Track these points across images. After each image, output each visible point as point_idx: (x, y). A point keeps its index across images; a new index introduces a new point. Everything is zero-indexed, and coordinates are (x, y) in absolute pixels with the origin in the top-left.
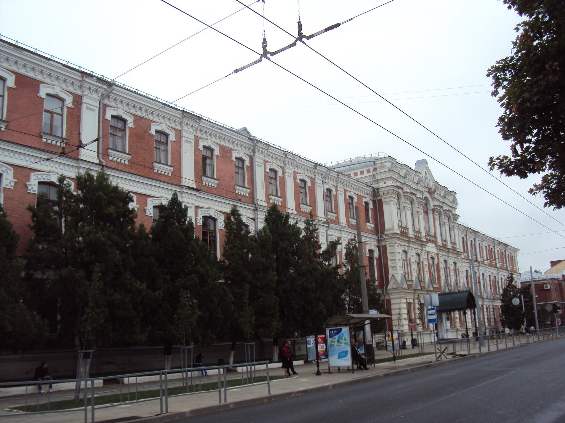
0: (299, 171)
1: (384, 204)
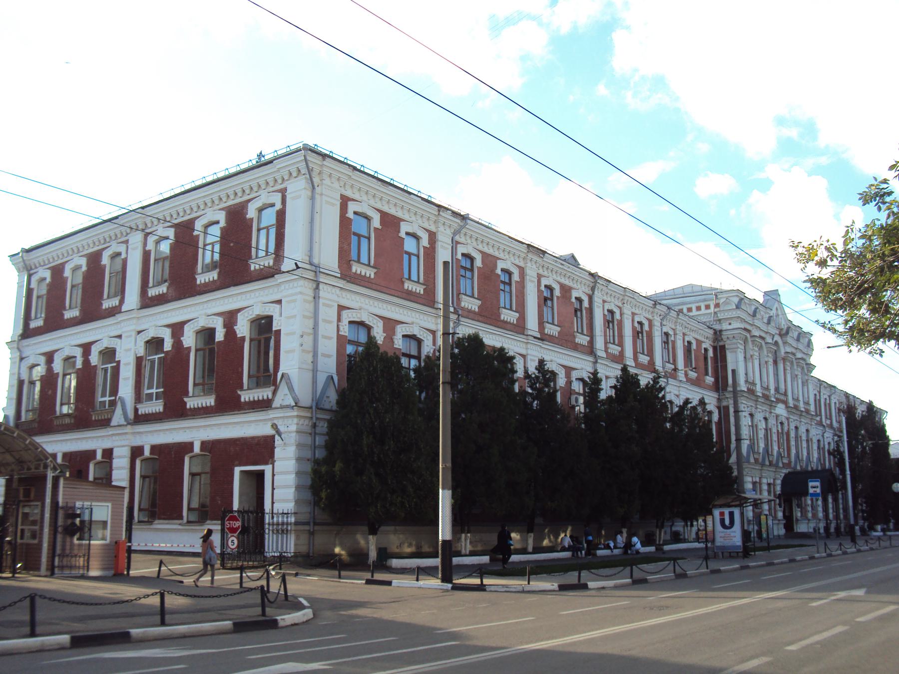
0: (545, 273)
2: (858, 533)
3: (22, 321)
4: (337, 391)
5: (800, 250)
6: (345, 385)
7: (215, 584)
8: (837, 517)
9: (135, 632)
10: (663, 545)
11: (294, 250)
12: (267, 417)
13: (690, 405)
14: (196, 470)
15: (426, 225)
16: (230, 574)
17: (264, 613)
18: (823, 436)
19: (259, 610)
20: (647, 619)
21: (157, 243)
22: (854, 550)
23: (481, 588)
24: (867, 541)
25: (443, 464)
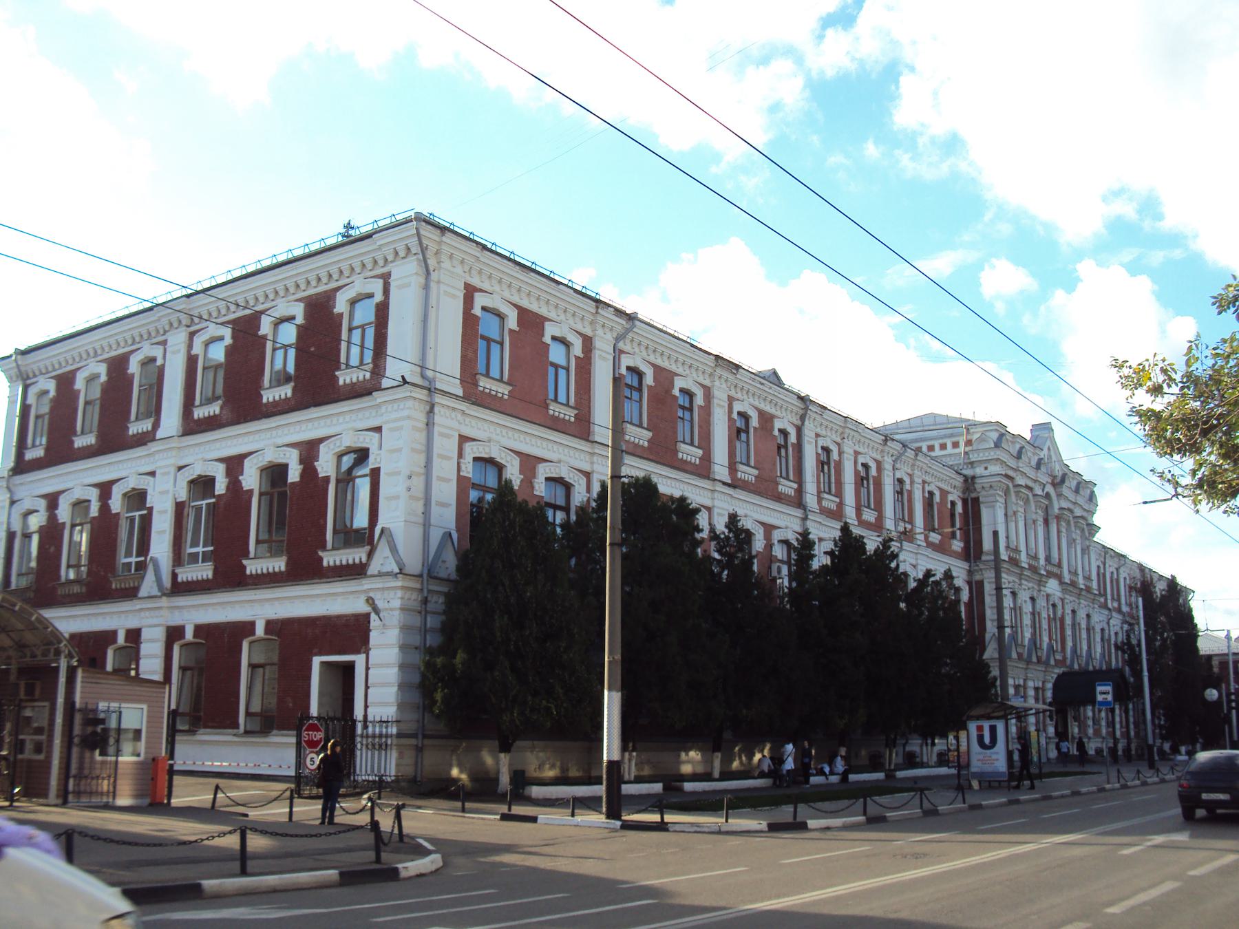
0: (739, 396)
1: (982, 506)
3: (13, 451)
4: (456, 553)
5: (1126, 371)
7: (294, 819)
8: (1126, 734)
9: (208, 884)
10: (895, 770)
13: (932, 579)
14: (259, 659)
15: (579, 327)
17: (378, 860)
19: (372, 855)
20: (904, 871)
21: (207, 344)
22: (1156, 779)
23: (662, 827)
24: (1172, 768)
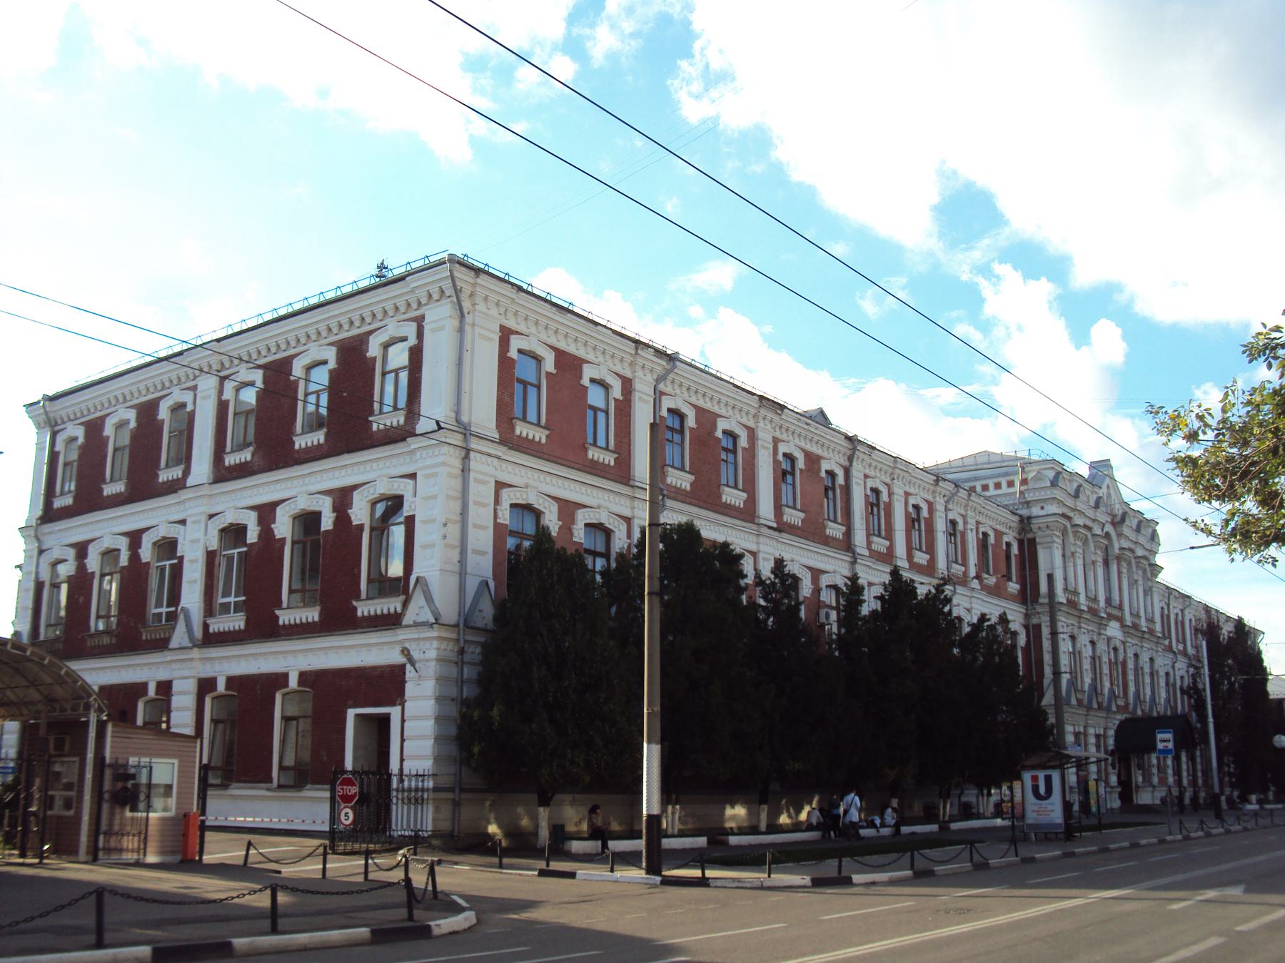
0: (784, 437)
2: (1224, 806)
4: (493, 602)
5: (1161, 417)
6: (505, 593)
7: (328, 874)
8: (1193, 783)
11: (434, 405)
12: (395, 639)
14: (291, 712)
15: (618, 369)
16: (340, 861)
17: (411, 918)
18: (1173, 667)
19: (403, 912)
23: (703, 882)
25: (648, 708)
